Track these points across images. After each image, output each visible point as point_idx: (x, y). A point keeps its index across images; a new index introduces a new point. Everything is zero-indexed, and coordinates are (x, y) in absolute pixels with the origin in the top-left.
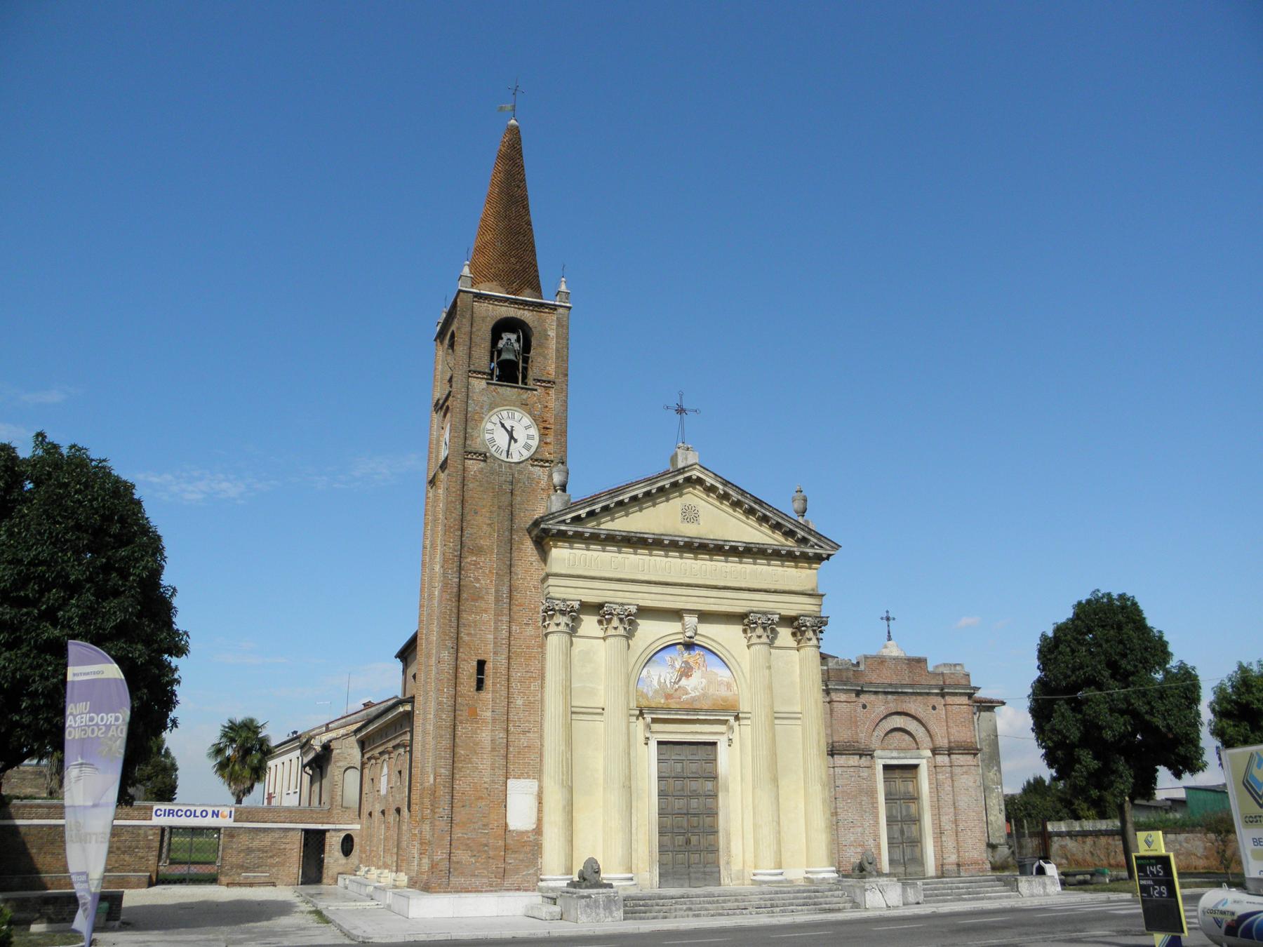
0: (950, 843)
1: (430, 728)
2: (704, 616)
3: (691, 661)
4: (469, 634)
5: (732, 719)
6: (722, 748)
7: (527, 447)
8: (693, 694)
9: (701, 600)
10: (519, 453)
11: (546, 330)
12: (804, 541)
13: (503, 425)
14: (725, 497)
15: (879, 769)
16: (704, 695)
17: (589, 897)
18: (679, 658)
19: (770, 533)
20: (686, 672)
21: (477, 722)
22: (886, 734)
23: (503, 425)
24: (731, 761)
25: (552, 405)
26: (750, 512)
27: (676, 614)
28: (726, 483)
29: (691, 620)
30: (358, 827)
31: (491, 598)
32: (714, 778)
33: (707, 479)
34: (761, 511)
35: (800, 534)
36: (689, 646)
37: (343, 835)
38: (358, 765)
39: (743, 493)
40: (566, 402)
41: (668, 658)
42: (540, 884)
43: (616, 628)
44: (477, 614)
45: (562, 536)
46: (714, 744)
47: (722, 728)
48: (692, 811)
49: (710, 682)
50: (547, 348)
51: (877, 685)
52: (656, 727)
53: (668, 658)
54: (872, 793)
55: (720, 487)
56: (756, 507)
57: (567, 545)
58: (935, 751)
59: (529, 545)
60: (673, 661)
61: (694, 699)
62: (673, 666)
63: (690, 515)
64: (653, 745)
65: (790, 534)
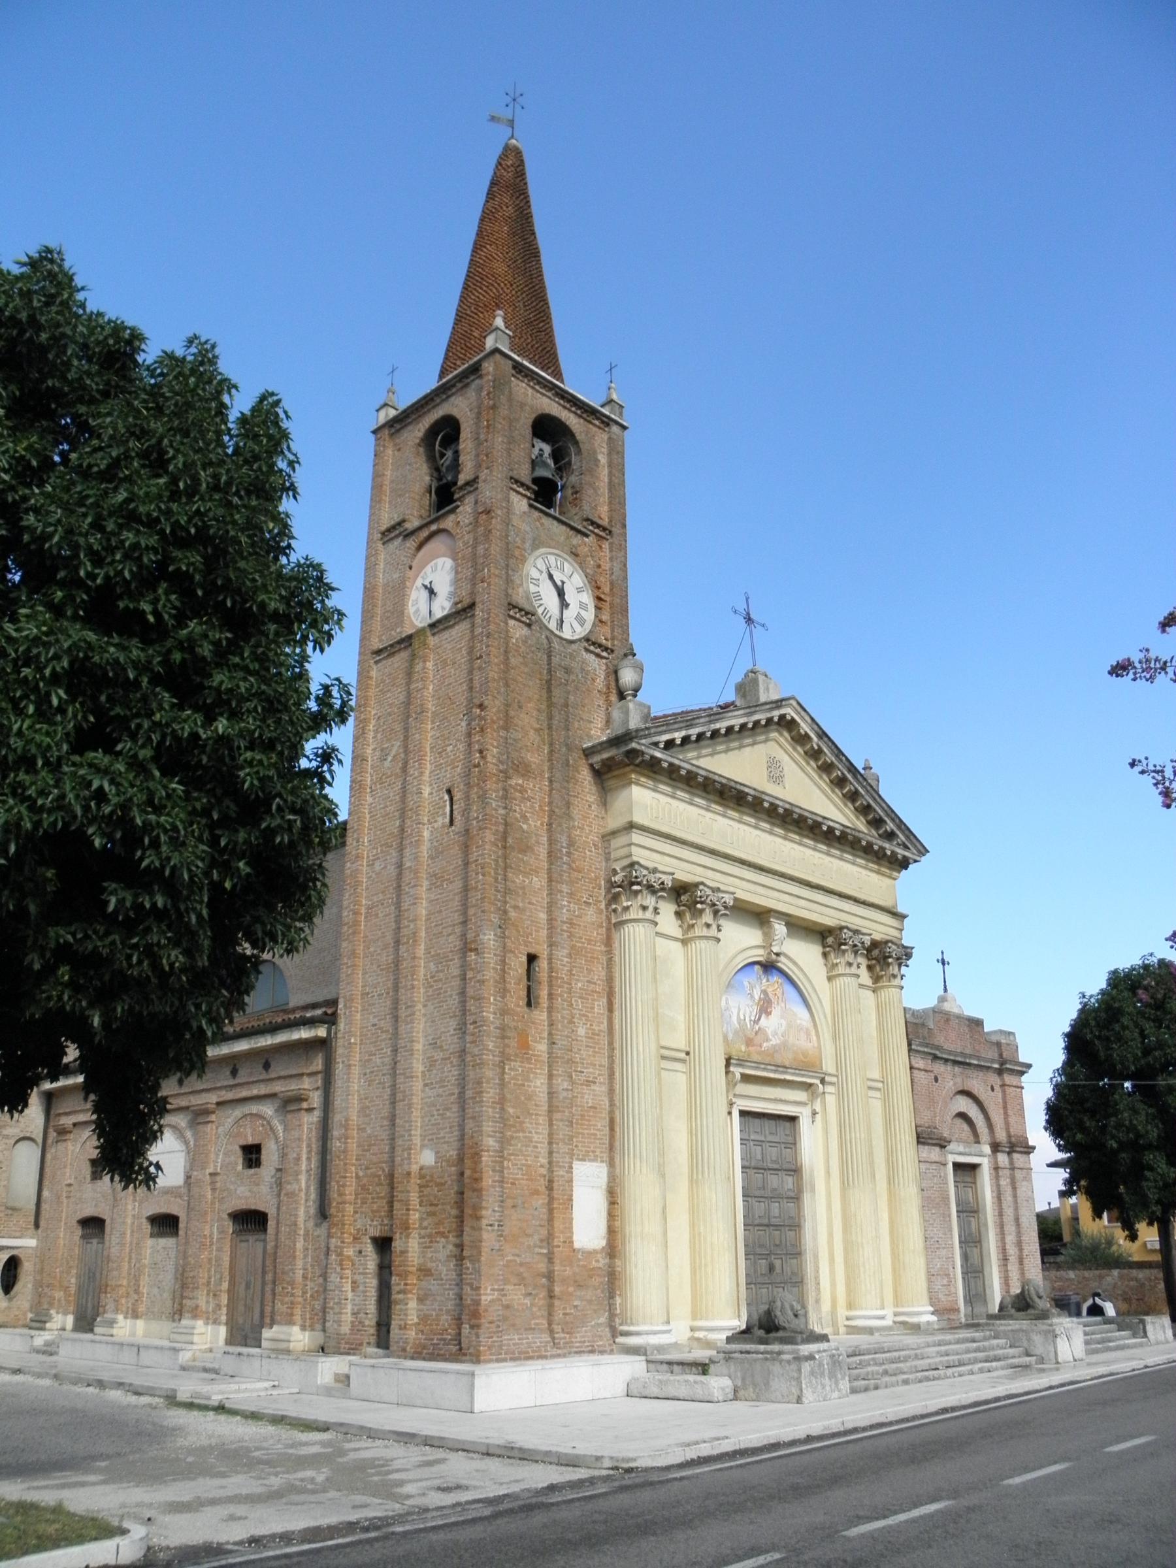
0: (1013, 1268)
1: (419, 1067)
2: (800, 928)
3: (769, 990)
4: (516, 907)
5: (817, 1082)
6: (804, 1123)
7: (580, 620)
8: (773, 1042)
9: (803, 903)
10: (573, 630)
11: (595, 452)
12: (890, 836)
13: (551, 577)
14: (815, 754)
15: (950, 1166)
16: (785, 1044)
17: (811, 1357)
18: (758, 983)
19: (852, 817)
20: (765, 1008)
21: (529, 1060)
22: (17, 1142)
23: (551, 577)
24: (814, 1145)
25: (606, 566)
26: (840, 782)
27: (760, 916)
28: (822, 735)
29: (780, 928)
30: (32, 1243)
31: (543, 851)
32: (795, 1171)
33: (802, 724)
34: (853, 784)
35: (890, 826)
36: (769, 967)
37: (5, 1257)
38: (38, 1135)
39: (839, 753)
40: (625, 565)
41: (746, 984)
42: (620, 1340)
43: (708, 926)
44: (526, 874)
45: (652, 768)
46: (793, 1119)
47: (801, 1096)
48: (774, 1221)
49: (789, 1026)
50: (598, 478)
51: (950, 1052)
52: (743, 1088)
53: (746, 984)
54: (946, 1199)
55: (815, 739)
56: (849, 776)
57: (650, 783)
58: (996, 1147)
59: (585, 775)
60: (752, 987)
61: (775, 1050)
62: (752, 997)
63: (775, 773)
64: (736, 1114)
65: (877, 823)
